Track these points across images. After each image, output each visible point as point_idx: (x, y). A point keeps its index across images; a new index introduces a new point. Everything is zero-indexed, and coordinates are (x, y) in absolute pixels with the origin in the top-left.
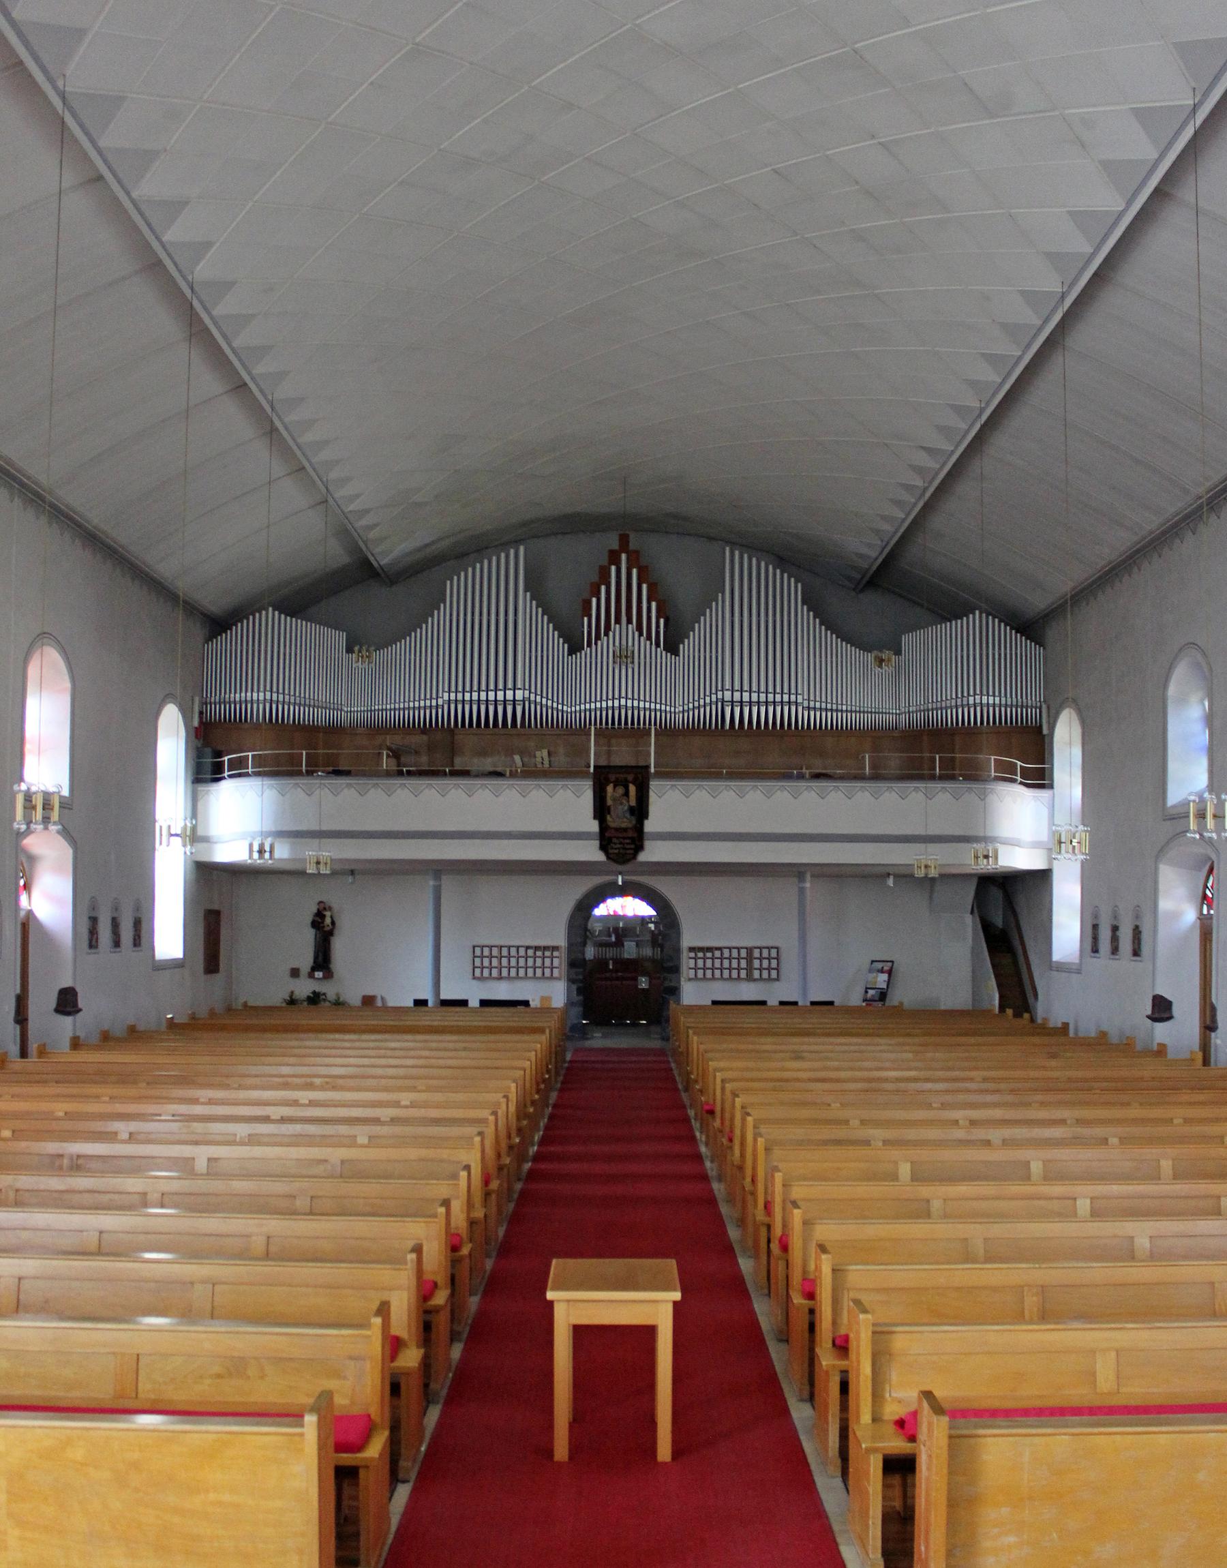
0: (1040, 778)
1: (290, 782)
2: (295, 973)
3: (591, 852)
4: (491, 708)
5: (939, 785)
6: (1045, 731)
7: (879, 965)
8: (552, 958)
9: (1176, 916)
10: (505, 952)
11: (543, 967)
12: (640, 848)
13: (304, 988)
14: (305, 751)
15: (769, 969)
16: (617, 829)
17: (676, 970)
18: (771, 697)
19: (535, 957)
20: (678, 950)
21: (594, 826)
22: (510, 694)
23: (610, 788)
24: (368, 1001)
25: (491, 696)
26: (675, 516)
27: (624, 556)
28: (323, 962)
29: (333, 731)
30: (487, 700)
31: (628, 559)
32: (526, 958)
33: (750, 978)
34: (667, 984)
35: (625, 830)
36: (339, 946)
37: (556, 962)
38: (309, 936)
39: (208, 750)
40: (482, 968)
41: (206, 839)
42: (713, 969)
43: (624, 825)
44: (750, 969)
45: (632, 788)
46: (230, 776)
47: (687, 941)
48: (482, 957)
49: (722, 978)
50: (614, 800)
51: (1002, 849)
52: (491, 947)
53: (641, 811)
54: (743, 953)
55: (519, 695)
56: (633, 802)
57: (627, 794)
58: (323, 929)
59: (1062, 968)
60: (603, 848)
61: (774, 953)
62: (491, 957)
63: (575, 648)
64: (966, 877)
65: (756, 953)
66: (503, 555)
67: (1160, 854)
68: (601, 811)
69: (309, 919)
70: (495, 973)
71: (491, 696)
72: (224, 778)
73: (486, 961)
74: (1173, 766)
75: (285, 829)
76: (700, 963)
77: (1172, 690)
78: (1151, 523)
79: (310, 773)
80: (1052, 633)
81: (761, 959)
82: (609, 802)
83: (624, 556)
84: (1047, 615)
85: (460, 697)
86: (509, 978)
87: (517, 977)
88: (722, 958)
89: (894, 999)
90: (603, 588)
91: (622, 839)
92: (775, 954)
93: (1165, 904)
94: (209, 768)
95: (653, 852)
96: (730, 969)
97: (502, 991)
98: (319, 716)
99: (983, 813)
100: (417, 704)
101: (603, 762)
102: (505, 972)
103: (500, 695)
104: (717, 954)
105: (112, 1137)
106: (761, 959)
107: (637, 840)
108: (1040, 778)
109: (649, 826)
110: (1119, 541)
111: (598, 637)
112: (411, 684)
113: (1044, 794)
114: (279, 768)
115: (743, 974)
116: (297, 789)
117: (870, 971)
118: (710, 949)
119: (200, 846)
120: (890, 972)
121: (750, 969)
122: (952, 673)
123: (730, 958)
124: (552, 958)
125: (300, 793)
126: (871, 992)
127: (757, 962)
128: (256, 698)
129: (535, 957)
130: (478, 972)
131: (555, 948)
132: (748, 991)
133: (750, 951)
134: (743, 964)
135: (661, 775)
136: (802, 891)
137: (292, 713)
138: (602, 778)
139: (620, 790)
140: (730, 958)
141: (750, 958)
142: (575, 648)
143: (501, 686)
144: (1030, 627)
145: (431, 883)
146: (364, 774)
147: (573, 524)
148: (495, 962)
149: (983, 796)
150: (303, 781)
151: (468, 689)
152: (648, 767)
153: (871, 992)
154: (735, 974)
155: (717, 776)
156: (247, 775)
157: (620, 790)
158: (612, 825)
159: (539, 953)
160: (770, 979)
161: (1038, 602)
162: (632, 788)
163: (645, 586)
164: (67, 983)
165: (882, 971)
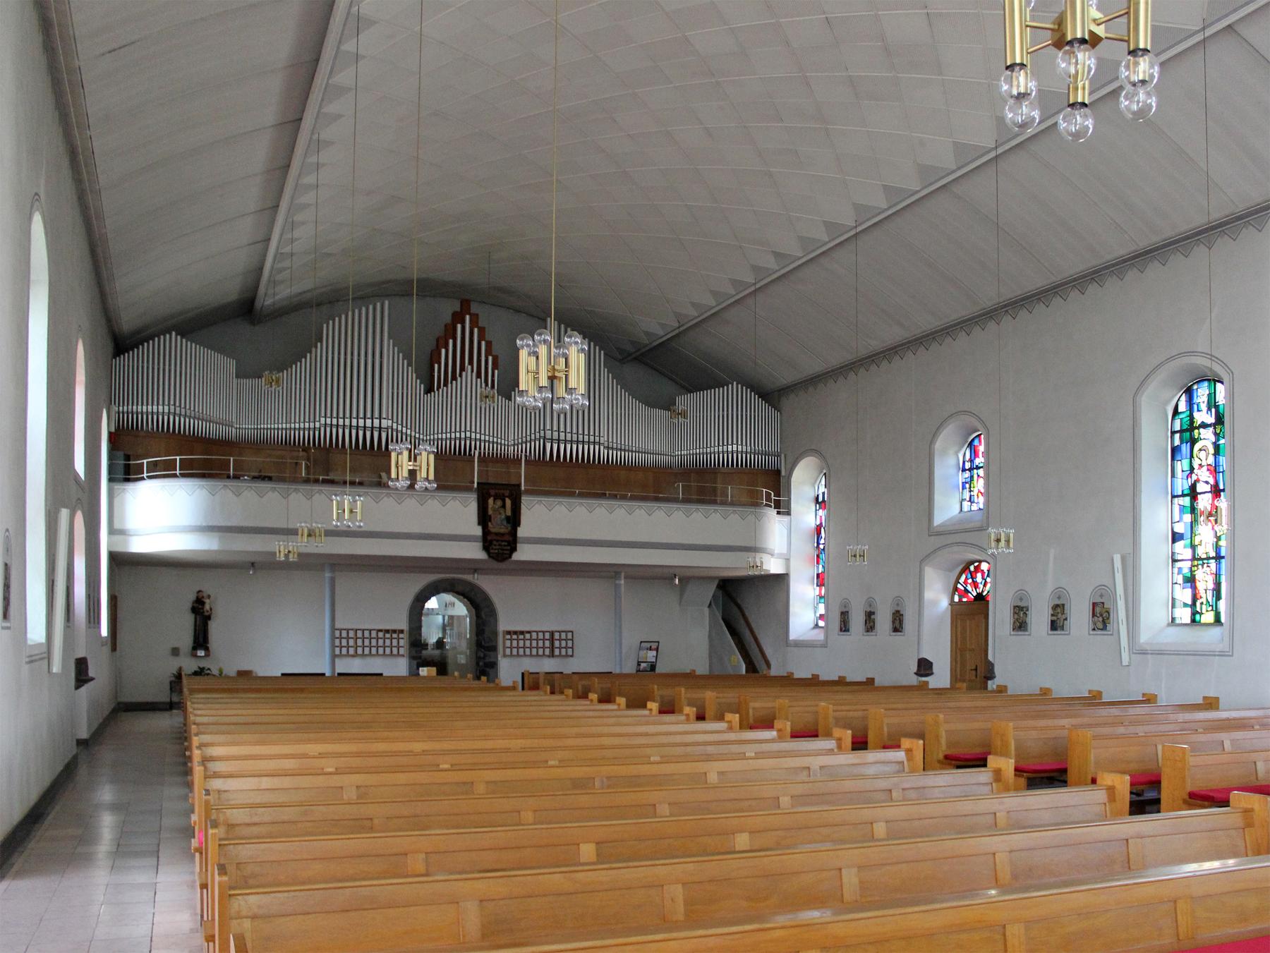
0: (783, 508)
1: (218, 484)
2: (175, 652)
3: (474, 552)
4: (361, 433)
5: (731, 509)
6: (783, 473)
7: (648, 645)
8: (398, 639)
9: (935, 603)
10: (359, 634)
11: (391, 647)
12: (514, 549)
13: (189, 665)
14: (204, 457)
15: (566, 648)
16: (496, 534)
17: (494, 649)
18: (562, 435)
19: (384, 639)
20: (495, 633)
21: (478, 531)
22: (376, 422)
23: (491, 501)
24: (244, 674)
25: (361, 422)
26: (501, 290)
27: (468, 317)
28: (201, 640)
29: (226, 445)
30: (372, 427)
31: (471, 321)
32: (378, 639)
33: (552, 655)
34: (487, 660)
35: (503, 535)
36: (214, 627)
37: (402, 642)
38: (188, 621)
39: (120, 454)
40: (364, 647)
41: (122, 532)
42: (531, 648)
43: (502, 531)
44: (552, 648)
45: (508, 502)
46: (150, 477)
47: (503, 626)
48: (341, 638)
49: (518, 655)
50: (494, 510)
51: (765, 558)
52: (348, 630)
53: (514, 520)
54: (547, 635)
55: (385, 423)
56: (509, 513)
57: (504, 506)
58: (201, 612)
59: (799, 644)
60: (486, 548)
61: (570, 636)
62: (348, 638)
63: (429, 390)
64: (711, 578)
65: (557, 636)
66: (371, 307)
67: (924, 560)
68: (484, 519)
69: (189, 605)
70: (352, 651)
71: (361, 422)
72: (143, 479)
73: (342, 641)
74: (938, 498)
75: (215, 524)
76: (515, 643)
77: (938, 445)
78: (928, 323)
79: (236, 477)
80: (788, 403)
81: (560, 640)
82: (490, 512)
83: (468, 317)
84: (788, 387)
85: (369, 423)
86: (363, 655)
87: (370, 654)
88: (531, 640)
89: (660, 669)
90: (451, 341)
91: (500, 542)
92: (570, 636)
93: (929, 595)
94: (121, 469)
95: (524, 553)
96: (537, 648)
97: (356, 666)
98: (214, 430)
99: (756, 530)
100: (312, 425)
101: (484, 481)
102: (360, 651)
103: (369, 423)
104: (528, 636)
105: (742, 757)
106: (560, 640)
107: (511, 542)
108: (783, 508)
109: (521, 532)
110: (893, 334)
111: (454, 378)
112: (287, 410)
113: (785, 519)
114: (194, 470)
115: (547, 652)
116: (224, 491)
117: (640, 648)
118: (522, 633)
119: (116, 538)
120: (657, 650)
121: (552, 648)
122: (717, 429)
123: (537, 640)
124: (398, 639)
125: (229, 494)
126: (643, 665)
127: (555, 643)
128: (154, 410)
129: (384, 639)
130: (570, 636)
131: (402, 631)
132: (549, 665)
133: (552, 633)
134: (547, 644)
135: (529, 492)
136: (617, 587)
137: (188, 425)
138: (484, 493)
139: (499, 503)
140: (537, 640)
141: (552, 640)
142: (429, 390)
143: (369, 415)
144: (771, 396)
145: (328, 575)
146: (282, 480)
147: (429, 288)
148: (351, 642)
149: (759, 518)
150: (229, 483)
151: (361, 415)
152: (519, 485)
153: (643, 665)
154: (541, 652)
155: (572, 495)
156: (175, 476)
157: (499, 503)
158: (493, 530)
159: (388, 636)
160: (567, 656)
161: (786, 377)
162: (508, 502)
163: (483, 343)
164: (81, 655)
165: (650, 649)
